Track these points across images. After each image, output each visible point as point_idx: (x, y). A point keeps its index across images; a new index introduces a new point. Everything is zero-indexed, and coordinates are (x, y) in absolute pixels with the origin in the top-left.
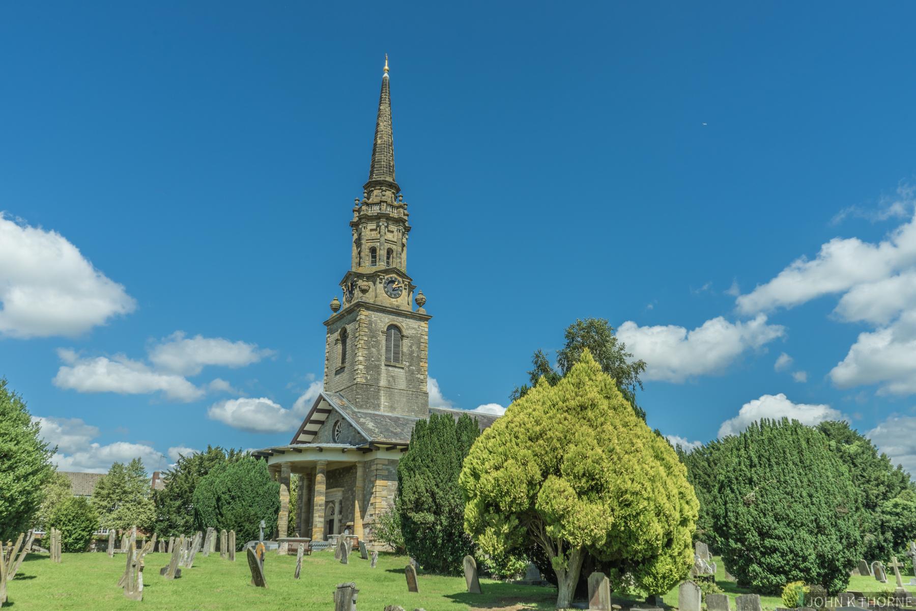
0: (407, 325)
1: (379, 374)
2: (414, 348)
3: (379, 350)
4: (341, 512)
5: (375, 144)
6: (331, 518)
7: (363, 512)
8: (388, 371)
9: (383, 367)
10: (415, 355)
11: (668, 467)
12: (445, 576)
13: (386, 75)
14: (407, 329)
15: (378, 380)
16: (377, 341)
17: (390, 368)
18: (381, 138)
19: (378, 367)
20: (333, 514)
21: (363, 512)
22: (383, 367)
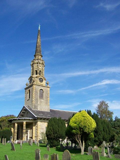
5: (37, 45)
8: (40, 100)
13: (39, 29)
22: (39, 100)
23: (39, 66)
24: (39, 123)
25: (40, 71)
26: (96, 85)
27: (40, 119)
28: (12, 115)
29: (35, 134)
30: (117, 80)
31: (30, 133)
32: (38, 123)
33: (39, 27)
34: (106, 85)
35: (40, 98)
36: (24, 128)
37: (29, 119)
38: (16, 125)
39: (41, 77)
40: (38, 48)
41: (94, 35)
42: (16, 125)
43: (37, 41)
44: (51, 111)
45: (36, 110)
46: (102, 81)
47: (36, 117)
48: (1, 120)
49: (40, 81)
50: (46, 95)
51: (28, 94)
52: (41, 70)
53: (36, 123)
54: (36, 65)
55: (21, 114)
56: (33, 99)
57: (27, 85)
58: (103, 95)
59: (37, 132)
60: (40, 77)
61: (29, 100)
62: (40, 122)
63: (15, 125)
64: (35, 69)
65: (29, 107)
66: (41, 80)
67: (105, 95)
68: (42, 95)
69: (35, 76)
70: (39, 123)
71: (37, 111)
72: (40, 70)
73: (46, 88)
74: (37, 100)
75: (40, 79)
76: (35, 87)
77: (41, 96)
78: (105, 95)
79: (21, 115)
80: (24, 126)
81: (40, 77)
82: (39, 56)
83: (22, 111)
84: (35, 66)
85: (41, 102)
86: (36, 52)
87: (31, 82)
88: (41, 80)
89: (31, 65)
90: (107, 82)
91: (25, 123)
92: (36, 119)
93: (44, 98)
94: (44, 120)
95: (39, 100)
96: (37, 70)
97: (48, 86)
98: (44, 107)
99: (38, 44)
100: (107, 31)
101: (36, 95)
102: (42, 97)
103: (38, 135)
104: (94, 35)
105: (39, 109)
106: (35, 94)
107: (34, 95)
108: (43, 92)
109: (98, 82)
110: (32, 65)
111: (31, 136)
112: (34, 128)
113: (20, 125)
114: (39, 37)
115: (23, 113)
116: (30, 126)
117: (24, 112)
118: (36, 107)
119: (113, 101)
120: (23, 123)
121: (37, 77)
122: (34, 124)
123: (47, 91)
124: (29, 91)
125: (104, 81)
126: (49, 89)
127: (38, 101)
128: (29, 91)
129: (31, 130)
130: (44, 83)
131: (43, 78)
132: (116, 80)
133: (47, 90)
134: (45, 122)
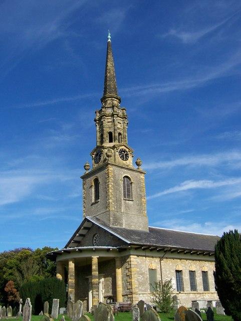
5: (106, 76)
8: (125, 203)
13: (109, 40)
18: (109, 73)
22: (123, 202)
23: (116, 123)
24: (134, 259)
25: (120, 134)
26: (171, 191)
27: (136, 249)
28: (27, 247)
29: (124, 288)
30: (210, 181)
31: (105, 287)
32: (132, 259)
33: (109, 37)
34: (190, 190)
35: (125, 199)
36: (95, 273)
37: (108, 250)
38: (72, 265)
39: (123, 147)
40: (110, 81)
41: (160, 90)
42: (72, 265)
43: (107, 66)
44: (151, 230)
45: (119, 227)
46: (182, 184)
47: (129, 242)
48: (21, 256)
49: (121, 158)
50: (138, 190)
51: (93, 190)
52: (122, 132)
53: (124, 260)
54: (110, 120)
55: (75, 239)
56: (110, 201)
57: (87, 167)
58: (184, 212)
59: (128, 284)
60: (121, 148)
61: (96, 203)
62: (136, 257)
63: (70, 267)
64: (107, 130)
65: (97, 219)
66: (124, 156)
67: (189, 211)
68: (129, 191)
69: (107, 144)
70: (134, 259)
71: (121, 229)
72: (119, 131)
73: (136, 174)
74: (118, 201)
75: (122, 151)
76: (113, 172)
77: (128, 194)
78: (189, 211)
79: (76, 242)
80: (95, 267)
81: (121, 148)
82: (114, 99)
83: (81, 232)
84: (107, 122)
85: (127, 207)
86: (105, 92)
87: (100, 159)
88: (124, 156)
89: (95, 120)
90: (192, 185)
91: (95, 259)
92: (125, 250)
93: (134, 199)
94: (144, 252)
95: (123, 202)
96: (112, 130)
97: (141, 168)
98: (135, 221)
99: (109, 73)
100: (213, 74)
101: (116, 189)
102: (129, 195)
103: (133, 291)
104: (160, 90)
105: (124, 224)
106: (113, 186)
107: (110, 191)
108: (132, 183)
109: (173, 186)
110: (100, 122)
111: (110, 294)
112: (119, 272)
113: (84, 269)
114: (109, 56)
115: (81, 235)
116: (107, 267)
117: (88, 232)
118: (117, 220)
119: (206, 223)
120: (91, 259)
121: (114, 147)
122: (118, 263)
123: (139, 182)
124: (96, 181)
125: (185, 182)
126: (142, 176)
127: (121, 205)
128: (96, 181)
129: (110, 279)
130: (130, 162)
131: (127, 150)
132: (208, 181)
133: (139, 179)
134: (146, 256)
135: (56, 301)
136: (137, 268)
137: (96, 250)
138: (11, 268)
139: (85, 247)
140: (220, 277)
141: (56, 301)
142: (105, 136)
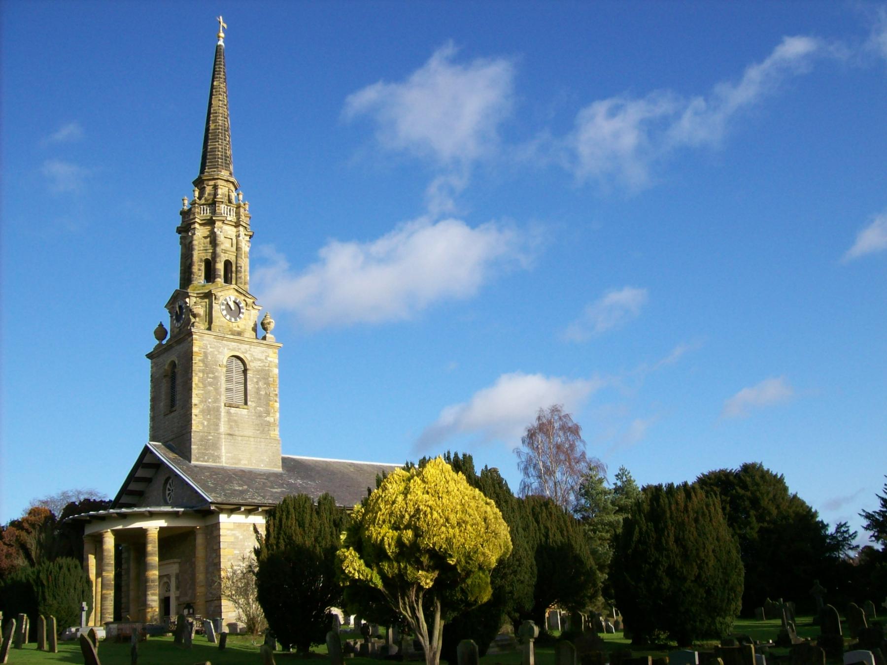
0: (252, 355)
1: (219, 419)
2: (261, 384)
3: (216, 390)
4: (177, 588)
5: (207, 129)
6: (167, 595)
7: (696, 496)
8: (228, 413)
9: (223, 410)
10: (263, 393)
11: (27, 531)
12: (713, 473)
13: (221, 42)
14: (252, 361)
15: (217, 425)
16: (215, 378)
17: (233, 410)
18: (215, 121)
19: (217, 410)
20: (168, 590)
21: (696, 496)
22: (223, 410)
38: (109, 541)
42: (109, 541)
64: (199, 254)
80: (153, 547)
96: (233, 259)
127: (218, 418)
135: (844, 619)
136: (235, 548)
137: (152, 516)
138: (10, 545)
139: (143, 509)
140: (402, 565)
141: (844, 619)
142: (195, 269)
